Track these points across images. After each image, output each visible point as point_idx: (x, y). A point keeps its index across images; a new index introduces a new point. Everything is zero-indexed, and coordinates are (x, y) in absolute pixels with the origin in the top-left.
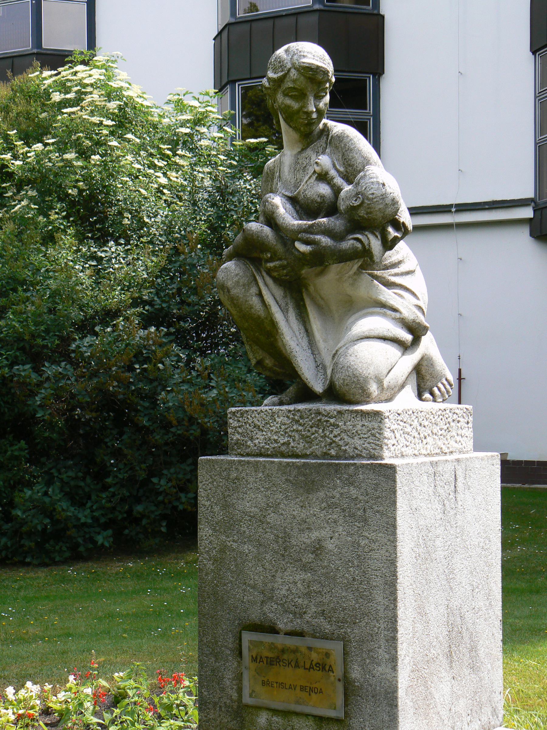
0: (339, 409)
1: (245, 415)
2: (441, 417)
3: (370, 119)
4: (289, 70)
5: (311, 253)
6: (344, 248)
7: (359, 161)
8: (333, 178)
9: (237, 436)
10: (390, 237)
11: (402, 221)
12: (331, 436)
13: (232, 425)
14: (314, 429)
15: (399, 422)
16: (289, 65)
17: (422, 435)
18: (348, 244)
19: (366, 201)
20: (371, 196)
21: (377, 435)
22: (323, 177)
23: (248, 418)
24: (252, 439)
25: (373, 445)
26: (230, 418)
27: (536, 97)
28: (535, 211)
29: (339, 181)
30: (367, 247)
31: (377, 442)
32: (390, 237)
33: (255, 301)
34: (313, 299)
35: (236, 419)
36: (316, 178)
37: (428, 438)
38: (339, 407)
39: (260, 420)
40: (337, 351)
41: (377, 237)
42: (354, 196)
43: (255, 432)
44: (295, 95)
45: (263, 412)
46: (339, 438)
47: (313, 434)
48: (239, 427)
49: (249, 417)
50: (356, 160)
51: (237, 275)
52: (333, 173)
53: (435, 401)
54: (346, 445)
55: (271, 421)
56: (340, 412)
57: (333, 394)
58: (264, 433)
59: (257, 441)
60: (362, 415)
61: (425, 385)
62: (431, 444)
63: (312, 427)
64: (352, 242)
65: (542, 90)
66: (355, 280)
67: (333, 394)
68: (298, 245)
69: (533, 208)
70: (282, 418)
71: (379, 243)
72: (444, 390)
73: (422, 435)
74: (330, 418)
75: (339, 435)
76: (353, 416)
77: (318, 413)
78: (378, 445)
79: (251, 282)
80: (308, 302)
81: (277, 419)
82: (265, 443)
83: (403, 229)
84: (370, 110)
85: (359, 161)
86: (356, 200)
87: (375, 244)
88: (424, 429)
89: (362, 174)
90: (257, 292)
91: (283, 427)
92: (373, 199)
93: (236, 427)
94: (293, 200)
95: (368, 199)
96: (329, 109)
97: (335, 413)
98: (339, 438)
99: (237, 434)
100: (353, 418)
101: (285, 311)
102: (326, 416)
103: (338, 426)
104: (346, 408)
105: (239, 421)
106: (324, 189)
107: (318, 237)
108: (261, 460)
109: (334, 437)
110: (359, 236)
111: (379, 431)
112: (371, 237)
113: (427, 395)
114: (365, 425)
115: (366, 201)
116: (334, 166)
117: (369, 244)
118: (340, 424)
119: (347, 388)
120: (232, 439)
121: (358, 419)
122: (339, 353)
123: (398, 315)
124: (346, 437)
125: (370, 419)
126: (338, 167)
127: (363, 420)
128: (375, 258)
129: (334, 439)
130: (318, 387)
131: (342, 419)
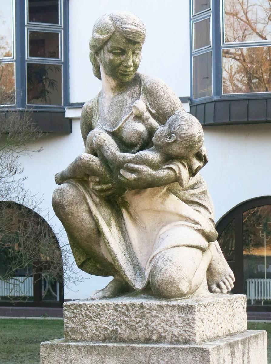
0: (159, 304)
1: (79, 308)
2: (229, 306)
3: (61, 32)
4: (114, 32)
5: (135, 180)
6: (161, 176)
7: (168, 105)
8: (147, 119)
9: (72, 325)
10: (195, 167)
11: (203, 154)
12: (153, 324)
13: (68, 316)
14: (138, 319)
15: (206, 313)
16: (113, 29)
17: (219, 322)
18: (163, 173)
19: (179, 139)
20: (183, 135)
21: (192, 325)
22: (139, 118)
23: (81, 310)
24: (85, 327)
25: (187, 332)
26: (66, 310)
27: (191, 19)
28: (191, 107)
29: (153, 122)
30: (178, 175)
31: (191, 330)
32: (195, 167)
33: (85, 216)
34: (129, 213)
35: (70, 311)
36: (134, 118)
37: (222, 323)
38: (158, 302)
39: (91, 311)
40: (154, 257)
41: (185, 166)
42: (168, 135)
43: (87, 322)
44: (118, 53)
45: (94, 305)
46: (160, 327)
47: (137, 323)
48: (74, 317)
49: (82, 309)
50: (166, 105)
51: (71, 195)
52: (147, 114)
53: (222, 293)
54: (166, 332)
55: (101, 313)
56: (161, 306)
57: (152, 290)
58: (95, 322)
59: (89, 329)
60: (178, 309)
61: (212, 280)
62: (224, 327)
63: (136, 317)
64: (166, 171)
65: (195, 14)
66: (164, 199)
67: (152, 290)
68: (122, 172)
69: (190, 104)
70: (110, 311)
71: (187, 171)
72: (229, 284)
73: (219, 322)
74: (151, 310)
75: (159, 324)
76: (171, 309)
77: (142, 307)
78: (192, 332)
79: (82, 201)
80: (125, 215)
81: (107, 312)
82: (96, 330)
83: (204, 160)
84: (61, 24)
85: (168, 105)
86: (170, 138)
87: (185, 173)
88: (220, 316)
89: (174, 117)
90: (87, 209)
91: (111, 317)
92: (184, 137)
93: (71, 318)
94: (116, 135)
95: (181, 137)
96: (28, 22)
97: (156, 307)
98: (160, 327)
99: (71, 323)
100: (171, 311)
101: (109, 224)
102: (148, 309)
103: (158, 317)
104: (164, 302)
105: (74, 313)
106: (141, 127)
107: (140, 167)
108: (96, 345)
109: (155, 325)
110: (171, 166)
111: (193, 322)
112: (181, 166)
113: (215, 287)
114: (181, 317)
115: (179, 139)
116: (148, 108)
117: (180, 173)
118: (160, 315)
119: (165, 287)
120: (67, 327)
121: (175, 312)
122: (155, 258)
123: (199, 227)
124: (165, 326)
125: (185, 312)
126: (151, 109)
127: (179, 312)
128: (184, 183)
129: (155, 327)
130: (139, 285)
131: (162, 311)
